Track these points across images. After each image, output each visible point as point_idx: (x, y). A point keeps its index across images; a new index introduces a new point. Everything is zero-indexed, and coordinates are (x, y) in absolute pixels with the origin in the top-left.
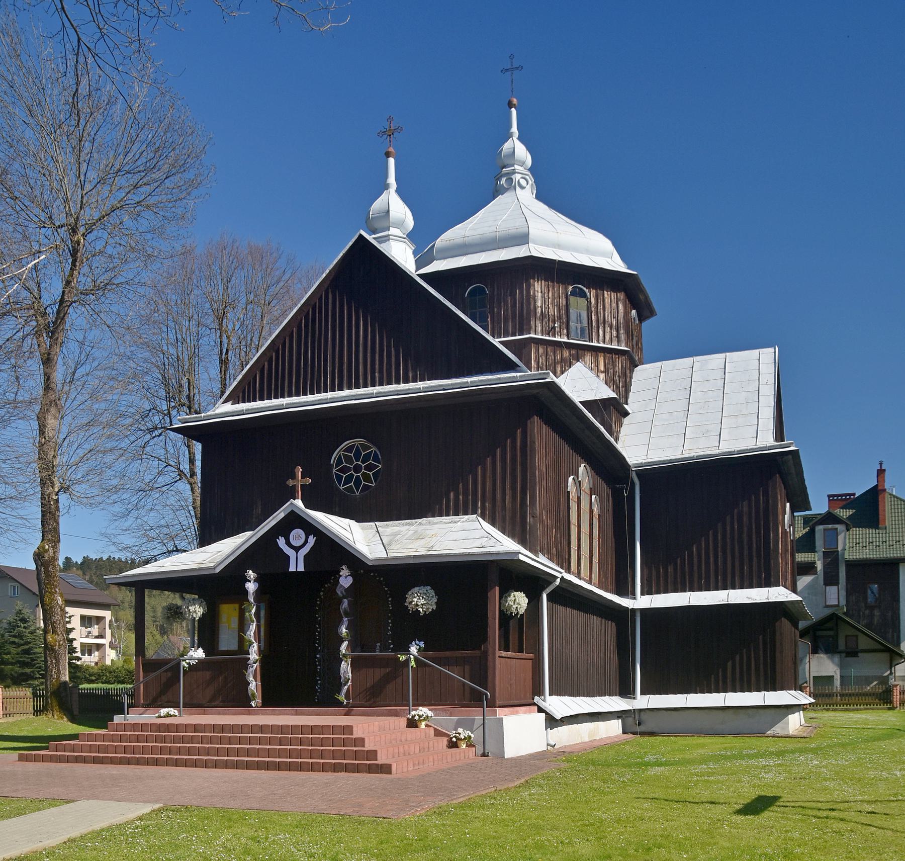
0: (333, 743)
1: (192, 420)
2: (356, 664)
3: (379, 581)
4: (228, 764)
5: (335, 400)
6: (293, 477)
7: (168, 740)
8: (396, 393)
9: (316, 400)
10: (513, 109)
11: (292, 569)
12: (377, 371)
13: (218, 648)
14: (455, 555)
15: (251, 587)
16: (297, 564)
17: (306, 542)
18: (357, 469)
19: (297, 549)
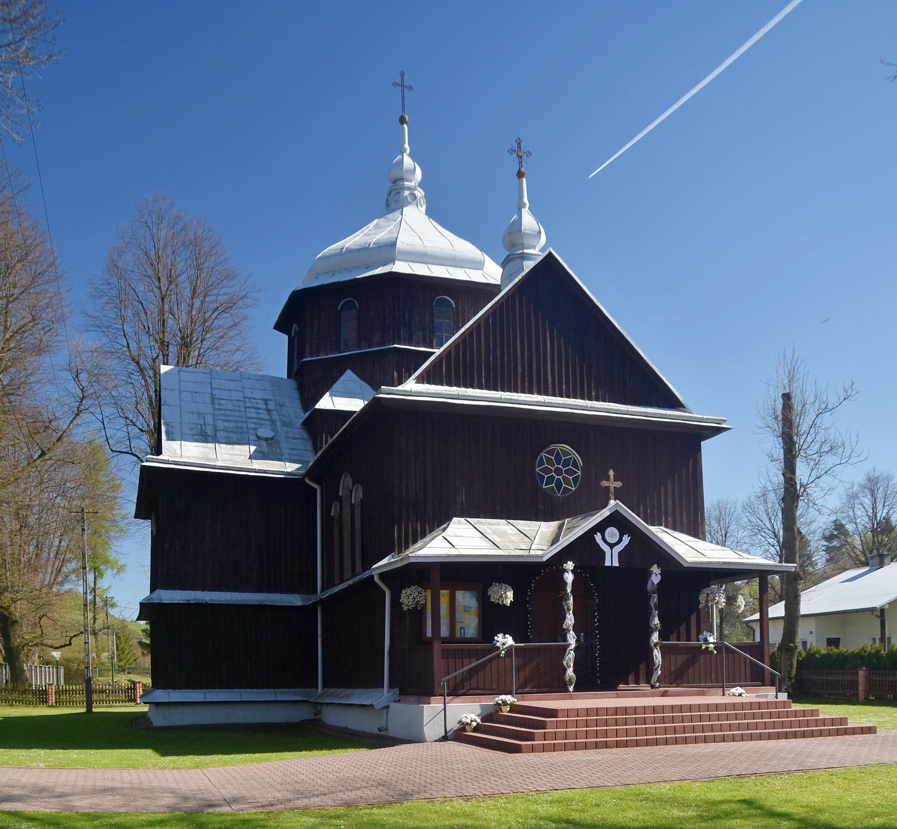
0: (771, 715)
1: (398, 393)
2: (664, 650)
3: (585, 577)
4: (753, 737)
5: (551, 405)
6: (607, 479)
7: (648, 721)
8: (607, 411)
9: (534, 401)
10: (405, 125)
11: (608, 563)
12: (564, 383)
13: (455, 635)
14: (718, 563)
15: (569, 577)
16: (612, 560)
17: (620, 540)
18: (558, 472)
19: (612, 546)
